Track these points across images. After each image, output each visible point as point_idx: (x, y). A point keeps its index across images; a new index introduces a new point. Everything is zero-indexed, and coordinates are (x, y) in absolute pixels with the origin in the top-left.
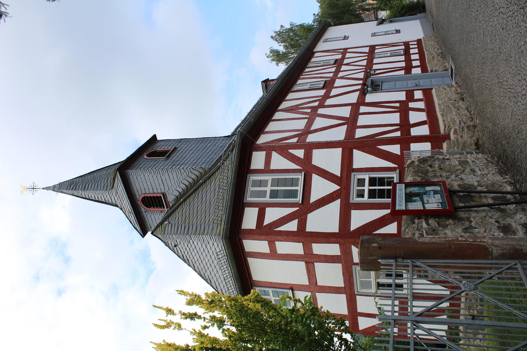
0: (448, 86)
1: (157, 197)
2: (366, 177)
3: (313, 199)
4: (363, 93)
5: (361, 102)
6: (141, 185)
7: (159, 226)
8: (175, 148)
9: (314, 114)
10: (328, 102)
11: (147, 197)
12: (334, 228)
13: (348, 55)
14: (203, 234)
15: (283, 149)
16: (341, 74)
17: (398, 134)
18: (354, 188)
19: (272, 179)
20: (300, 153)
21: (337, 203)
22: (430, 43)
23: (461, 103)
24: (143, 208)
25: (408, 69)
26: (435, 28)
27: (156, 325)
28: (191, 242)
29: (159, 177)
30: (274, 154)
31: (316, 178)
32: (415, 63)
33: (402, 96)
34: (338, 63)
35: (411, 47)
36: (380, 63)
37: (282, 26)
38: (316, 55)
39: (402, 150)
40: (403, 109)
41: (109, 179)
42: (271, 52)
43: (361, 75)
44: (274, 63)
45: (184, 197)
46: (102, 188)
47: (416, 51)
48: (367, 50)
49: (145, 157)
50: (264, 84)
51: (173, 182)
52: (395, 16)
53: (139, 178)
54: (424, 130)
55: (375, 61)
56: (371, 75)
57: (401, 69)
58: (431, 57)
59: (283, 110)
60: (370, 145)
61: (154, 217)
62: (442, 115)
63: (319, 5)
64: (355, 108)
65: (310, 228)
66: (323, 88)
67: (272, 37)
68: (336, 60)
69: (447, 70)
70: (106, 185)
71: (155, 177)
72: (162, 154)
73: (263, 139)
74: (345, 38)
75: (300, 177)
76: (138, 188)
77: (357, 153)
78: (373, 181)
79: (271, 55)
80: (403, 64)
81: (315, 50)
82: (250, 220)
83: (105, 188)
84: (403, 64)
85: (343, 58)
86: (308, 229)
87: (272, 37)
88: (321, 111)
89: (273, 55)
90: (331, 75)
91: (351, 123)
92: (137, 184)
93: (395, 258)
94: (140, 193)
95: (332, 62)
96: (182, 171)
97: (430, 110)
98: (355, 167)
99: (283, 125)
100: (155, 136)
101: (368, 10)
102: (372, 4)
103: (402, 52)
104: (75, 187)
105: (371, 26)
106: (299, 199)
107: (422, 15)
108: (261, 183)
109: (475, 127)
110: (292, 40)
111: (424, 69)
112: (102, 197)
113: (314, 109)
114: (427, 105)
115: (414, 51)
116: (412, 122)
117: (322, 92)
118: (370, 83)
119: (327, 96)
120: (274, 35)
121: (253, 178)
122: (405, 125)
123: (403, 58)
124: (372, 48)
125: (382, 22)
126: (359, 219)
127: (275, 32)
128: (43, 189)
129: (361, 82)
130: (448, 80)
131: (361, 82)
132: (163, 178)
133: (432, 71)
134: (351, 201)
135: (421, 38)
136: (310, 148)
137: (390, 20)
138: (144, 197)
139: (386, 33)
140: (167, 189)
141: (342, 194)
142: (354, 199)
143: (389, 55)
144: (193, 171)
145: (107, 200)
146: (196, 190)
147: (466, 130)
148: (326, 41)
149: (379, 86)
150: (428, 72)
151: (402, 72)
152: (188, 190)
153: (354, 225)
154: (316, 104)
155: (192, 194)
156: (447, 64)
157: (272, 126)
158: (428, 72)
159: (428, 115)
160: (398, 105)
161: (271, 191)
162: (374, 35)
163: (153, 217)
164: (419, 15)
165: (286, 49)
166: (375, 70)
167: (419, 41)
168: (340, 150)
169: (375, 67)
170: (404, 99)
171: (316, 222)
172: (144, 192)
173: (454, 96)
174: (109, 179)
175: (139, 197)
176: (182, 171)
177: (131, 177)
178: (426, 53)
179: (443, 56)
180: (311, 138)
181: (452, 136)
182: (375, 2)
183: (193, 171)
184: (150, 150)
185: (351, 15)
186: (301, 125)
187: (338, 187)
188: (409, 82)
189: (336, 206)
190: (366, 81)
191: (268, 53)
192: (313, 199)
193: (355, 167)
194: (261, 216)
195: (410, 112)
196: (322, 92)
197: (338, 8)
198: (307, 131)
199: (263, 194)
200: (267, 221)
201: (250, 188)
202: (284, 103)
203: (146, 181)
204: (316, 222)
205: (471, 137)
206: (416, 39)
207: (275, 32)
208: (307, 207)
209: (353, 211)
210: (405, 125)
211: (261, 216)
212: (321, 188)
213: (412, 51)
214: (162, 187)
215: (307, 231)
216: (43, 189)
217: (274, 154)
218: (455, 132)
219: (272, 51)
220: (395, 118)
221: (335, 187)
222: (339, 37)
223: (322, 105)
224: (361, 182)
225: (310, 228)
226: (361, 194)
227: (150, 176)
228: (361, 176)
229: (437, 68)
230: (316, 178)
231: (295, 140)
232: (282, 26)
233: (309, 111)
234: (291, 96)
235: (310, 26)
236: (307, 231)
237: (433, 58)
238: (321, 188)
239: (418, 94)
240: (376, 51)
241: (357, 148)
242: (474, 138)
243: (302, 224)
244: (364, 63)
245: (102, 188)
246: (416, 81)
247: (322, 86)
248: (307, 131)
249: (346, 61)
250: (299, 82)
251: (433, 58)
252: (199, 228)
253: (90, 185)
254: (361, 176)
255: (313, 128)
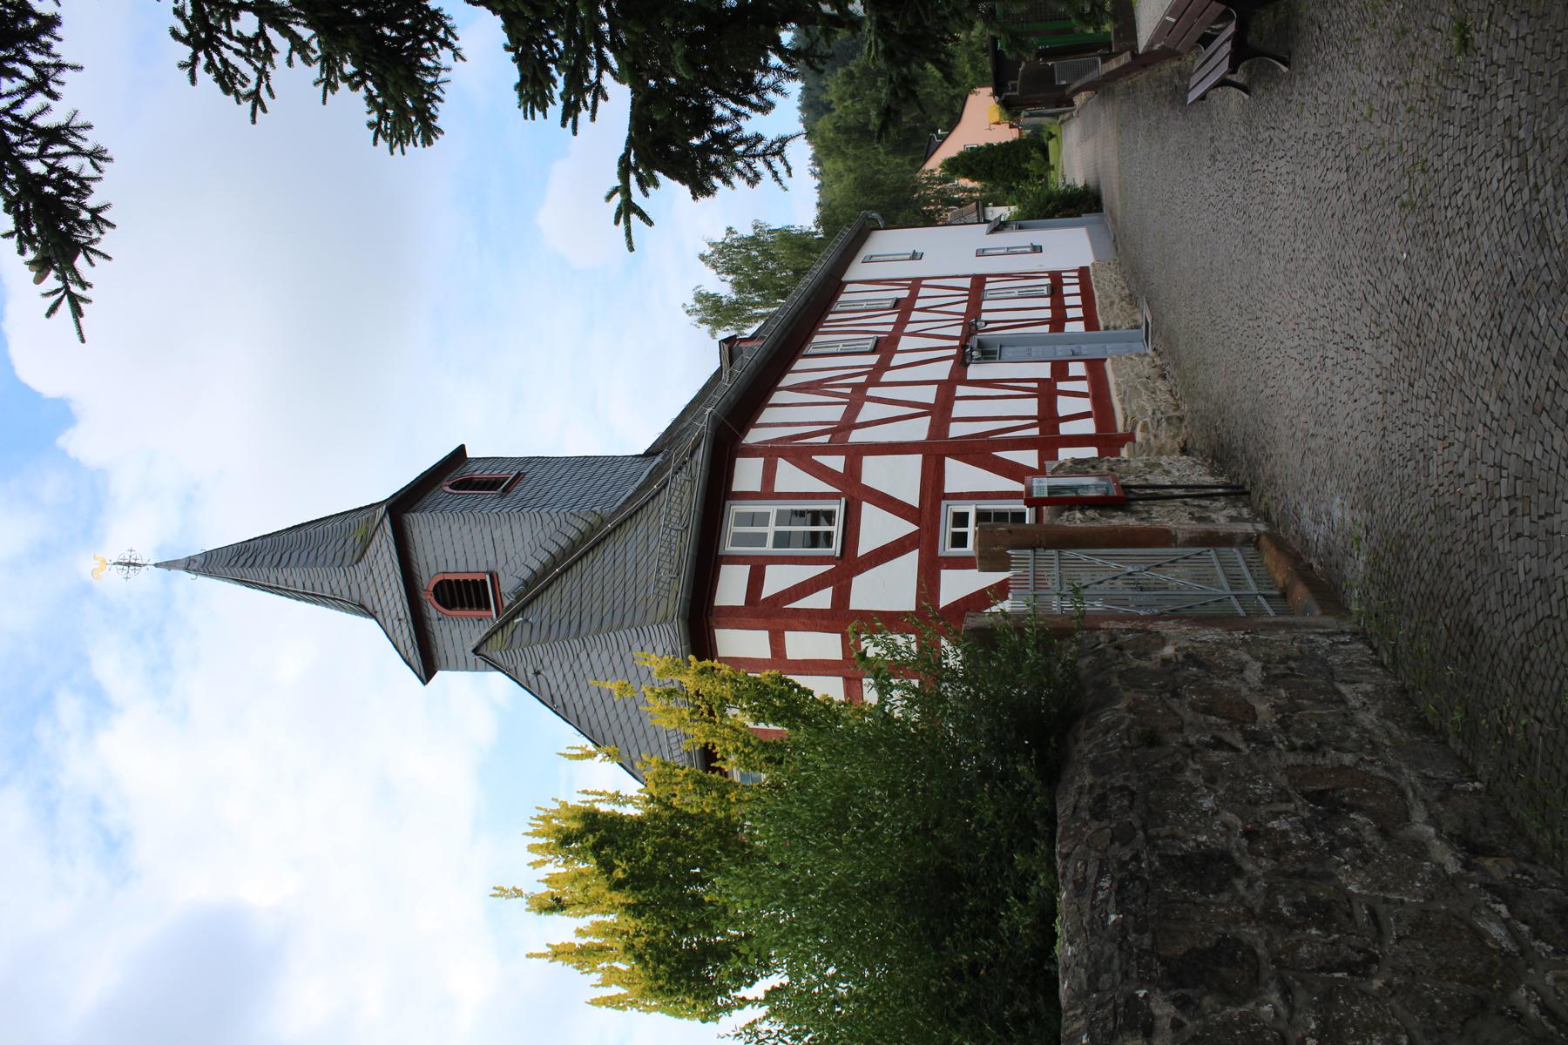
0: (1139, 355)
1: (474, 581)
2: (971, 509)
3: (864, 548)
4: (962, 361)
5: (958, 376)
6: (439, 551)
7: (495, 632)
8: (519, 474)
9: (857, 397)
10: (887, 376)
11: (449, 581)
12: (909, 604)
13: (923, 292)
14: (621, 626)
15: (801, 454)
16: (909, 328)
17: (1035, 432)
18: (947, 530)
19: (779, 512)
20: (837, 463)
21: (913, 557)
22: (1107, 275)
23: (1159, 383)
24: (433, 610)
25: (1058, 321)
26: (1121, 246)
27: (565, 755)
28: (583, 656)
29: (487, 531)
30: (783, 466)
31: (868, 511)
32: (1070, 313)
33: (1044, 371)
34: (904, 308)
35: (1065, 281)
36: (994, 310)
37: (730, 230)
38: (849, 288)
39: (1041, 460)
40: (1046, 393)
41: (350, 541)
42: (698, 300)
43: (957, 331)
44: (706, 328)
45: (537, 585)
46: (329, 561)
47: (1077, 289)
48: (967, 283)
49: (447, 489)
50: (726, 347)
51: (519, 544)
52: (1031, 217)
53: (436, 533)
54: (1088, 427)
55: (985, 305)
56: (977, 330)
57: (1042, 322)
58: (1107, 302)
59: (789, 389)
60: (979, 451)
61: (456, 630)
62: (1122, 401)
63: (817, 182)
64: (946, 392)
65: (857, 602)
66: (873, 352)
67: (702, 257)
68: (897, 302)
69: (1137, 327)
70: (340, 554)
71: (476, 531)
72: (490, 484)
73: (754, 437)
74: (915, 256)
75: (836, 507)
76: (430, 558)
77: (953, 467)
78: (982, 516)
79: (698, 306)
80: (1048, 314)
81: (845, 278)
82: (732, 587)
83: (338, 561)
84: (1048, 314)
85: (914, 296)
86: (855, 604)
87: (702, 257)
88: (871, 392)
89: (704, 309)
90: (890, 328)
91: (940, 412)
92: (428, 548)
93: (1034, 548)
94: (433, 572)
95: (889, 304)
96: (546, 518)
97: (1099, 393)
98: (947, 490)
99: (789, 413)
100: (462, 449)
101: (959, 203)
102: (971, 190)
103: (1045, 291)
104: (250, 561)
105: (976, 235)
106: (836, 548)
107: (1093, 217)
108: (753, 519)
109: (1181, 419)
110: (756, 267)
111: (1090, 322)
112: (326, 584)
113: (859, 389)
114: (1093, 385)
115: (1071, 289)
116: (1062, 412)
117: (873, 359)
118: (974, 345)
119: (883, 366)
120: (708, 251)
121: (736, 508)
122: (1048, 417)
123: (1047, 302)
124: (979, 281)
125: (999, 227)
126: (956, 585)
127: (712, 244)
128: (156, 565)
129: (957, 343)
130: (1139, 347)
131: (957, 343)
132: (497, 534)
133: (1106, 328)
134: (941, 553)
135: (1088, 264)
136: (854, 455)
137: (1018, 223)
138: (440, 583)
139: (1010, 252)
140: (502, 562)
141: (923, 541)
142: (946, 549)
143: (1016, 293)
144: (571, 519)
145: (337, 591)
146: (597, 544)
147: (1164, 424)
148: (869, 260)
149: (994, 353)
150: (1098, 329)
151: (1046, 328)
152: (555, 564)
153: (947, 596)
154: (862, 379)
155: (586, 553)
156: (1138, 316)
157: (767, 415)
158: (1098, 329)
159: (1095, 403)
160: (1035, 385)
161: (777, 533)
162: (981, 253)
163: (456, 632)
164: (1085, 217)
165: (739, 292)
166: (987, 323)
167: (1083, 273)
168: (919, 457)
169: (985, 316)
170: (1048, 375)
171: (868, 592)
172: (442, 568)
173: (1148, 371)
174: (350, 541)
175: (427, 581)
176: (546, 518)
177: (416, 531)
178: (1097, 294)
179: (1132, 300)
180: (856, 436)
181: (1139, 436)
182: (976, 184)
183: (571, 519)
184: (456, 476)
185: (916, 213)
186: (836, 413)
187: (914, 528)
188: (1059, 348)
189: (909, 562)
190: (967, 339)
191: (690, 302)
192: (864, 548)
193: (947, 490)
194: (756, 581)
195: (1060, 398)
196: (873, 359)
197: (882, 193)
198: (848, 424)
199: (760, 539)
200: (768, 591)
201: (732, 528)
202: (789, 376)
203: (451, 543)
204: (868, 592)
205: (1174, 437)
206: (1077, 267)
207: (712, 244)
208: (849, 565)
209: (943, 572)
210: (1048, 417)
211: (756, 581)
212: (878, 528)
213: (1066, 290)
214: (491, 557)
215: (852, 607)
216: (156, 565)
217: (783, 466)
218: (1145, 428)
219: (702, 298)
220: (1031, 407)
221: (908, 528)
222: (892, 253)
223: (874, 381)
224: (961, 519)
225: (857, 602)
226: (959, 540)
227: (466, 529)
228: (960, 507)
229: (1118, 323)
230: (868, 511)
231: (825, 439)
232: (730, 230)
233: (849, 390)
234: (801, 364)
235: (808, 234)
236: (852, 607)
237: (1112, 304)
238: (878, 528)
239: (1076, 369)
240: (988, 286)
241: (950, 456)
242: (1180, 439)
243: (842, 596)
244: (963, 308)
245: (329, 561)
246: (1074, 347)
247: (869, 347)
248: (848, 424)
249: (919, 304)
250: (817, 339)
251: (1112, 304)
252: (608, 618)
253: (295, 556)
254: (960, 507)
255: (860, 419)
